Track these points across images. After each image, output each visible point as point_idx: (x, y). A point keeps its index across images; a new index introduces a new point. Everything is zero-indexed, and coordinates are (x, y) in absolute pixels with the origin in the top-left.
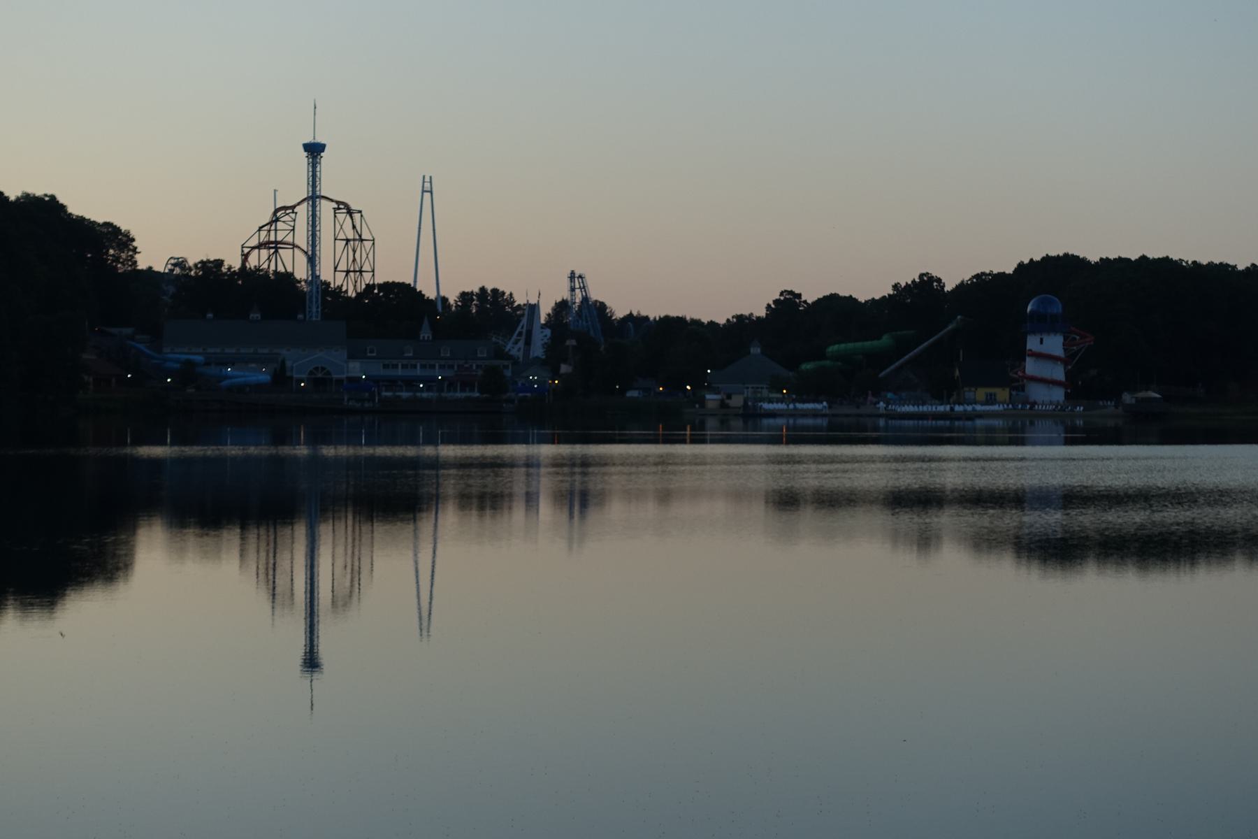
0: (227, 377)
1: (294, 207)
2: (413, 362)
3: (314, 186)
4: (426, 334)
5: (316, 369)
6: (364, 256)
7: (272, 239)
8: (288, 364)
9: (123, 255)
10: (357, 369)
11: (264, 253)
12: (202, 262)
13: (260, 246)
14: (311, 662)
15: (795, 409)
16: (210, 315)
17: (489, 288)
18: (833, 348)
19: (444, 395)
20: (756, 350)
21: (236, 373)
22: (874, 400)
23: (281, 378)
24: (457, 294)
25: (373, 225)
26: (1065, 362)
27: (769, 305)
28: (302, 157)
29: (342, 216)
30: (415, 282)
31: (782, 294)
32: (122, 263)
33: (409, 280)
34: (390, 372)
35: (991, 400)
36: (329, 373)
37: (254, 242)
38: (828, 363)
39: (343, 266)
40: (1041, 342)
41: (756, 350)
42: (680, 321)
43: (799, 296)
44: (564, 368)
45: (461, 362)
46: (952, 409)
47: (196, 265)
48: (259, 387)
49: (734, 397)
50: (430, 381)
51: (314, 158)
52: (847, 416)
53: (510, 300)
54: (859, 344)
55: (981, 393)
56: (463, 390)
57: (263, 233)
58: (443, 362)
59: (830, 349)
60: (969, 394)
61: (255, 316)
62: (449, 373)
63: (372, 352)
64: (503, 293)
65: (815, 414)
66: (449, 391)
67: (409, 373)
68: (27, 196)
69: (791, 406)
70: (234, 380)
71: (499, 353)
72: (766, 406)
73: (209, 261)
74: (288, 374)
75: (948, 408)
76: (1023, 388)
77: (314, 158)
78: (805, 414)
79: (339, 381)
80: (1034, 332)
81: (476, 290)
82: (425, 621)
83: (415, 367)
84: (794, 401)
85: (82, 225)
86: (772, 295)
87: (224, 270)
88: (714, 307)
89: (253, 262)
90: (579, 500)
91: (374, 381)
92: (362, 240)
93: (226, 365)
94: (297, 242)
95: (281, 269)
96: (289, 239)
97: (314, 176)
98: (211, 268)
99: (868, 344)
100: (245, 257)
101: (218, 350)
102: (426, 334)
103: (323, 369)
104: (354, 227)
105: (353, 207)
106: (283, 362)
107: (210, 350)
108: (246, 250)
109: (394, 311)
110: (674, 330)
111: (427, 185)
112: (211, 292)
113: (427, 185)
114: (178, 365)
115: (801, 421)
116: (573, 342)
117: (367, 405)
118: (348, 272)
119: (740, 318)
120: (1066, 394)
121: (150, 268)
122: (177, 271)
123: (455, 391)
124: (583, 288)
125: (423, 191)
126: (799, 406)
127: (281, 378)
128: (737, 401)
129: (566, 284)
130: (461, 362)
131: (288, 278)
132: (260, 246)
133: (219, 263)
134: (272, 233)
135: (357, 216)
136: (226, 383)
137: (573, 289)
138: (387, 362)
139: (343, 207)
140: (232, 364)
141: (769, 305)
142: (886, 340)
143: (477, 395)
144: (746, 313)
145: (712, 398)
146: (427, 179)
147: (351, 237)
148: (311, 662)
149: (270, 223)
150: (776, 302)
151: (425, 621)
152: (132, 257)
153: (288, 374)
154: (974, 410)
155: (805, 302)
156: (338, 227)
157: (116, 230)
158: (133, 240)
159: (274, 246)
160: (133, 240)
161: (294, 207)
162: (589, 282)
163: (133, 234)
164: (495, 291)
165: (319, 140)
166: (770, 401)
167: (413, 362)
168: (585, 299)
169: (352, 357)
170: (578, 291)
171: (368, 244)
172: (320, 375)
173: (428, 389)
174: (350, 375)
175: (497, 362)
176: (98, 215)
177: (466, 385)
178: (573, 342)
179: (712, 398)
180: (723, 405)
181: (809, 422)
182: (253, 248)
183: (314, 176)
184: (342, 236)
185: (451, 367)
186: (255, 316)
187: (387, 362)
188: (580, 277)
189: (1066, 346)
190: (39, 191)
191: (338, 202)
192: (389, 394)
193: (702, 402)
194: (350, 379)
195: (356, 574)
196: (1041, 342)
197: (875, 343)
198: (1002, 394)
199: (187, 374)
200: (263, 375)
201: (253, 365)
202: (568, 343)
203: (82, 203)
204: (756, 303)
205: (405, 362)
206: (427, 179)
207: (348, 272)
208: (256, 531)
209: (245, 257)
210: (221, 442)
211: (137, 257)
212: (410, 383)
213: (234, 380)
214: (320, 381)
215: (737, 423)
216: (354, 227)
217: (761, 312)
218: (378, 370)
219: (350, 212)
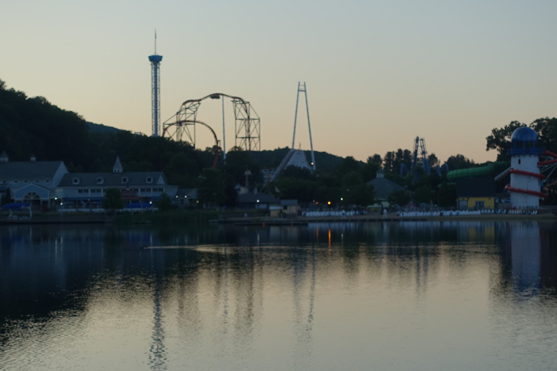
5: (30, 194)
17: (403, 149)
26: (540, 177)
28: (149, 63)
34: (83, 195)
35: (480, 206)
36: (38, 196)
40: (519, 162)
46: (441, 214)
49: (288, 207)
52: (415, 219)
55: (472, 202)
60: (462, 201)
63: (76, 181)
67: (145, 195)
75: (439, 213)
76: (508, 196)
80: (514, 155)
83: (100, 191)
90: (351, 269)
94: (197, 119)
96: (192, 118)
103: (34, 194)
105: (246, 100)
108: (166, 126)
120: (540, 201)
123: (82, 208)
126: (333, 213)
135: (247, 105)
137: (417, 147)
138: (81, 188)
146: (302, 83)
154: (458, 214)
165: (159, 53)
173: (66, 206)
181: (412, 224)
186: (33, 159)
188: (422, 140)
189: (540, 164)
191: (234, 98)
196: (519, 162)
198: (489, 202)
206: (302, 83)
208: (415, 262)
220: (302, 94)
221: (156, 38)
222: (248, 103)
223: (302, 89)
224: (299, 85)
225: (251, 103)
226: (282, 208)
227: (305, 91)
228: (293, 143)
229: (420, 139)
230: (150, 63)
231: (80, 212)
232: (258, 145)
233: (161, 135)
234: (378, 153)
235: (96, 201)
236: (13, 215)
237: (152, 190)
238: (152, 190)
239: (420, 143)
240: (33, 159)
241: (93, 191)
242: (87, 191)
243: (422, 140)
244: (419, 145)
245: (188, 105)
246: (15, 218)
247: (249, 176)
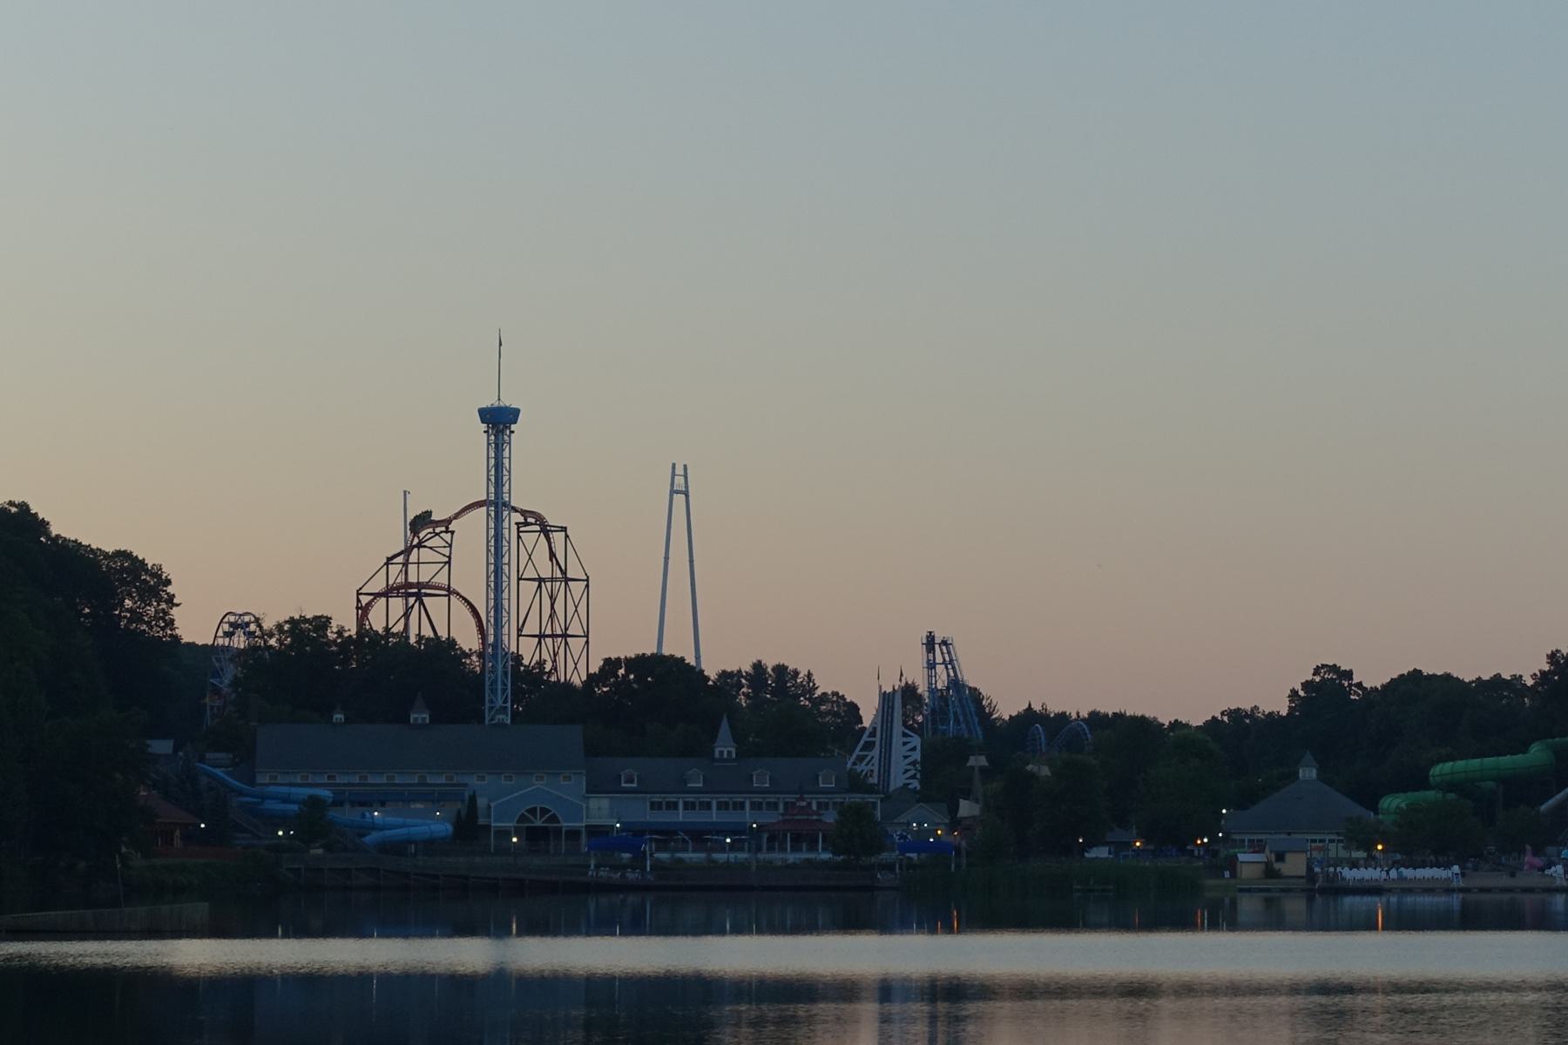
0: (374, 827)
1: (449, 521)
2: (705, 798)
3: (499, 484)
4: (725, 747)
5: (532, 811)
6: (571, 609)
7: (412, 579)
8: (481, 802)
10: (601, 811)
11: (397, 604)
12: (292, 621)
13: (387, 593)
15: (1401, 878)
16: (339, 717)
17: (769, 664)
18: (1441, 770)
19: (761, 856)
20: (1308, 773)
21: (390, 820)
22: (1538, 861)
23: (469, 828)
24: (1545, 659)
25: (588, 550)
27: (1294, 693)
30: (698, 658)
31: (1317, 671)
32: (148, 624)
33: (650, 650)
36: (554, 819)
37: (378, 585)
38: (1431, 795)
39: (532, 627)
41: (1308, 773)
42: (1143, 726)
43: (1349, 675)
44: (966, 808)
45: (791, 798)
47: (279, 627)
48: (430, 845)
49: (1288, 857)
53: (809, 687)
54: (1489, 761)
56: (795, 849)
57: (395, 569)
58: (757, 798)
59: (1437, 770)
62: (771, 818)
66: (771, 849)
67: (697, 817)
69: (1393, 874)
70: (388, 833)
71: (856, 783)
72: (1348, 874)
73: (304, 620)
74: (482, 821)
79: (574, 834)
81: (747, 668)
83: (708, 806)
84: (1396, 864)
85: (72, 556)
88: (1185, 697)
89: (377, 621)
91: (635, 834)
92: (567, 580)
95: (427, 632)
96: (442, 579)
97: (499, 466)
98: (307, 634)
99: (1506, 760)
101: (356, 780)
102: (725, 747)
103: (544, 811)
104: (552, 555)
106: (473, 799)
108: (365, 600)
109: (779, 715)
110: (1128, 739)
111: (679, 480)
112: (309, 673)
113: (679, 480)
114: (295, 807)
116: (982, 761)
117: (631, 876)
118: (541, 636)
119: (1235, 714)
122: (240, 642)
124: (950, 663)
125: (673, 492)
126: (1408, 873)
127: (469, 828)
128: (1294, 865)
130: (791, 798)
131: (443, 649)
132: (387, 593)
133: (322, 623)
134: (412, 569)
135: (558, 538)
136: (373, 837)
137: (931, 666)
138: (657, 798)
141: (1294, 693)
142: (1537, 754)
143: (826, 856)
144: (1247, 706)
146: (679, 470)
147: (546, 574)
149: (407, 552)
152: (166, 613)
153: (482, 821)
155: (1359, 685)
157: (138, 565)
158: (168, 582)
159: (414, 592)
160: (168, 582)
161: (449, 521)
164: (780, 670)
165: (508, 401)
166: (1354, 864)
167: (705, 798)
168: (955, 684)
169: (594, 789)
170: (940, 669)
171: (576, 588)
172: (538, 823)
174: (594, 822)
175: (857, 798)
178: (982, 761)
179: (1249, 862)
180: (1270, 872)
182: (377, 595)
183: (499, 466)
186: (420, 716)
187: (657, 798)
188: (944, 643)
191: (524, 513)
192: (664, 856)
193: (1232, 864)
194: (594, 831)
197: (1519, 758)
200: (438, 824)
201: (419, 806)
202: (972, 761)
205: (690, 798)
206: (679, 470)
207: (541, 636)
209: (363, 611)
211: (174, 611)
212: (699, 836)
213: (388, 833)
215: (1295, 906)
216: (552, 555)
218: (641, 812)
219: (545, 530)
223: (680, 489)
224: (674, 474)
226: (1273, 857)
227: (687, 496)
229: (938, 640)
230: (484, 427)
231: (681, 860)
232: (582, 666)
233: (352, 629)
235: (657, 832)
236: (597, 866)
237: (681, 806)
238: (681, 806)
241: (723, 806)
243: (944, 643)
244: (939, 659)
247: (982, 770)
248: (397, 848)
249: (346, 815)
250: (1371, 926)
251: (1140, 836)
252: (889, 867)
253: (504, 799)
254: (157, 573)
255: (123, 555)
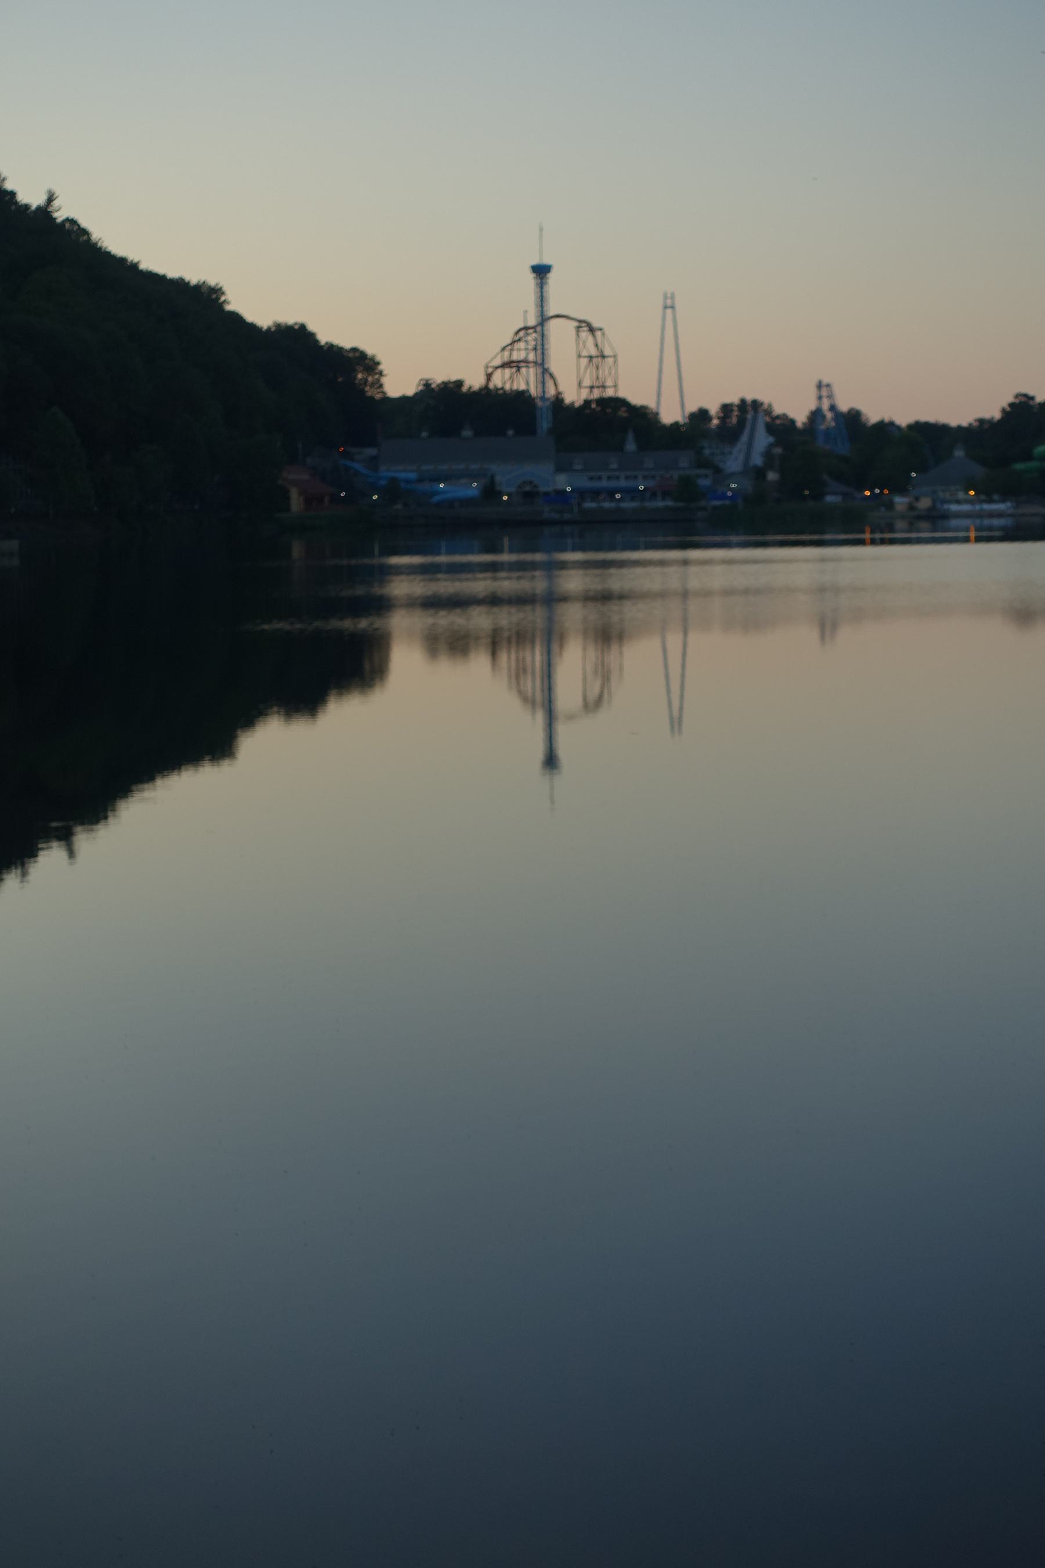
0: (443, 492)
4: (631, 446)
8: (498, 478)
9: (370, 379)
10: (564, 483)
11: (507, 372)
14: (551, 761)
17: (749, 397)
20: (959, 453)
23: (491, 492)
25: (615, 340)
28: (530, 278)
29: (585, 334)
37: (498, 362)
50: (631, 493)
51: (542, 279)
56: (663, 499)
61: (467, 433)
62: (651, 483)
64: (762, 404)
65: (1000, 515)
68: (278, 326)
72: (954, 507)
77: (542, 279)
78: (992, 515)
79: (547, 494)
82: (676, 723)
84: (982, 502)
85: (333, 352)
86: (1006, 399)
87: (465, 389)
89: (498, 380)
91: (582, 494)
92: (603, 357)
93: (439, 481)
100: (489, 376)
102: (631, 446)
103: (531, 482)
105: (595, 324)
106: (492, 478)
107: (424, 468)
108: (490, 370)
109: (609, 425)
112: (447, 408)
115: (987, 522)
118: (592, 387)
121: (427, 385)
124: (830, 396)
125: (666, 307)
126: (986, 507)
127: (491, 492)
129: (813, 393)
133: (459, 384)
135: (598, 334)
136: (436, 499)
137: (820, 398)
138: (593, 474)
139: (586, 326)
140: (445, 479)
145: (900, 502)
148: (551, 761)
149: (513, 342)
150: (1011, 405)
151: (676, 723)
152: (378, 380)
156: (581, 345)
158: (378, 364)
160: (378, 364)
162: (837, 390)
163: (379, 358)
165: (546, 261)
167: (617, 473)
169: (560, 469)
171: (610, 360)
176: (345, 341)
177: (666, 494)
180: (911, 508)
182: (497, 368)
184: (585, 353)
185: (653, 477)
186: (467, 433)
187: (593, 474)
188: (828, 386)
190: (290, 318)
191: (580, 321)
193: (890, 506)
195: (605, 675)
199: (393, 491)
203: (331, 331)
204: (989, 405)
209: (489, 376)
210: (438, 553)
211: (384, 380)
212: (611, 493)
214: (529, 495)
217: (997, 415)
219: (592, 330)
220: (669, 311)
221: (541, 236)
222: (601, 329)
223: (669, 305)
225: (606, 330)
228: (659, 395)
234: (705, 405)
239: (824, 392)
240: (510, 432)
242: (600, 478)
245: (522, 334)
246: (555, 516)
248: (451, 503)
249: (426, 486)
250: (966, 540)
251: (862, 489)
252: (704, 509)
253: (510, 477)
254: (372, 359)
255: (354, 350)
